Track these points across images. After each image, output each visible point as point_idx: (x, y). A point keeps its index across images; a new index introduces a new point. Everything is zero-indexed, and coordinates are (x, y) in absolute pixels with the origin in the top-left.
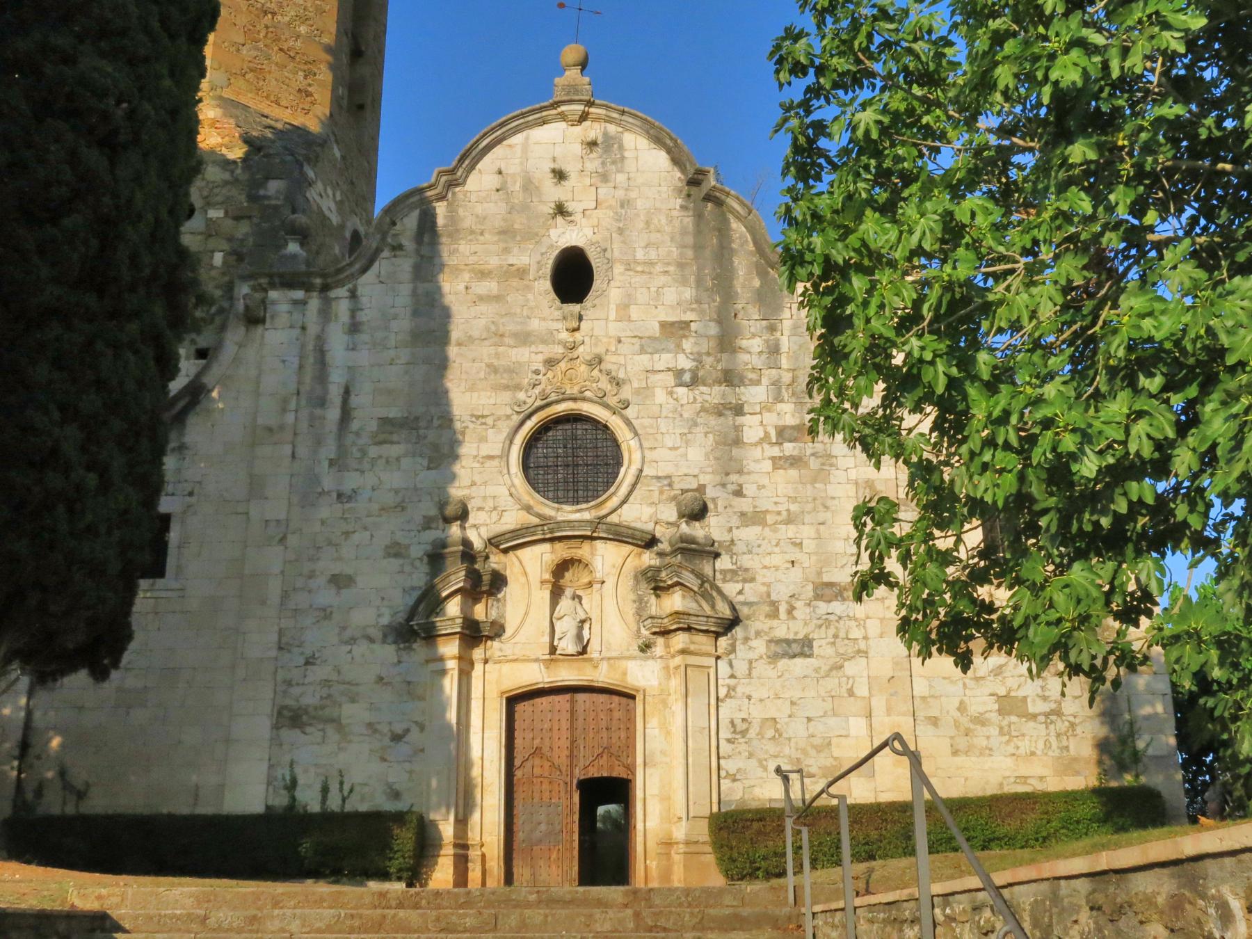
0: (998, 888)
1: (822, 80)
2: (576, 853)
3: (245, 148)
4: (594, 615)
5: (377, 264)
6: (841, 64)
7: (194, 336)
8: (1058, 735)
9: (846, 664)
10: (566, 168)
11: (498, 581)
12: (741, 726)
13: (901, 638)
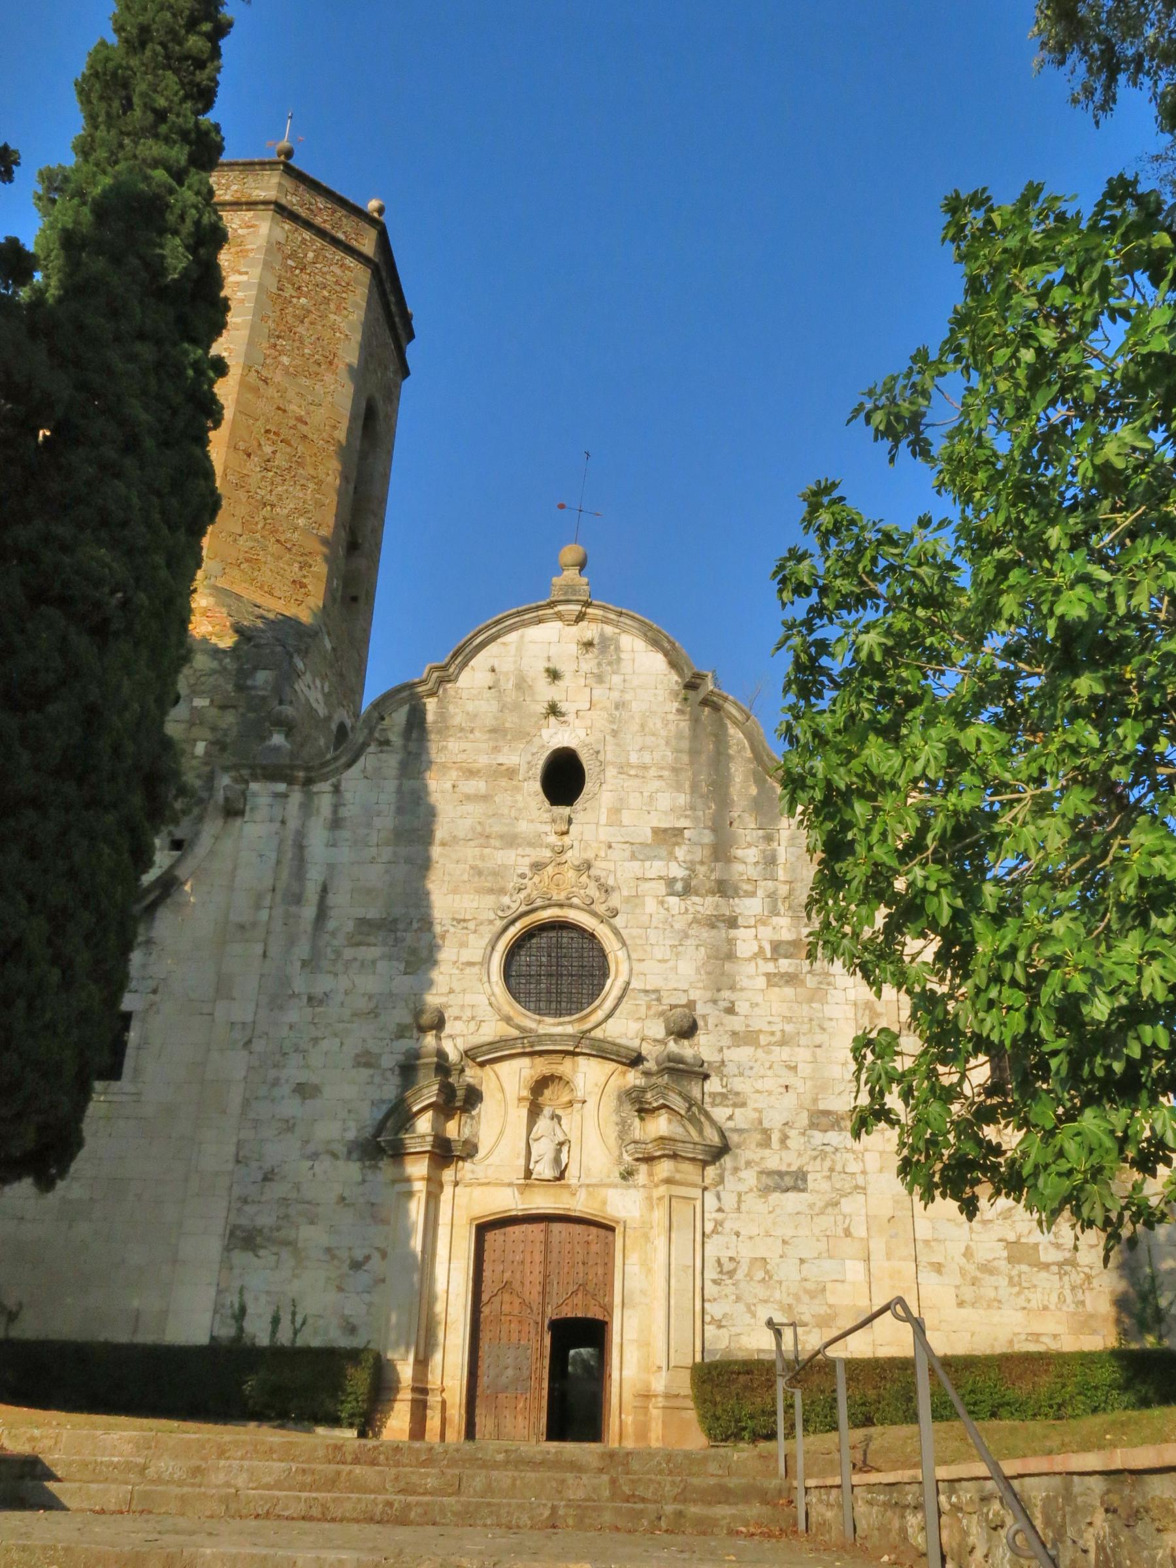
0: (1007, 1478)
1: (825, 601)
2: (545, 1403)
3: (235, 638)
4: (574, 1139)
5: (362, 759)
6: (844, 585)
7: (171, 828)
8: (1073, 1288)
9: (843, 1200)
10: (561, 667)
11: (473, 1097)
12: (728, 1266)
13: (903, 1180)
